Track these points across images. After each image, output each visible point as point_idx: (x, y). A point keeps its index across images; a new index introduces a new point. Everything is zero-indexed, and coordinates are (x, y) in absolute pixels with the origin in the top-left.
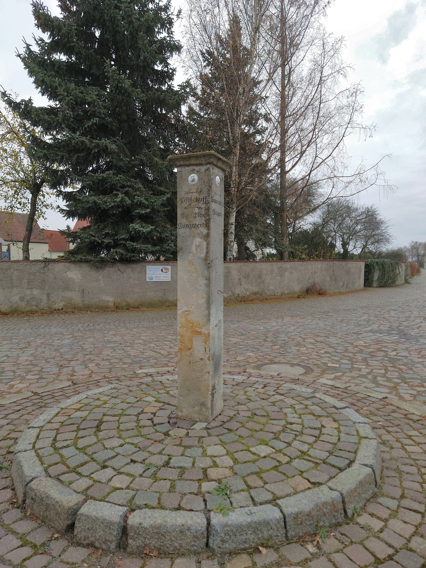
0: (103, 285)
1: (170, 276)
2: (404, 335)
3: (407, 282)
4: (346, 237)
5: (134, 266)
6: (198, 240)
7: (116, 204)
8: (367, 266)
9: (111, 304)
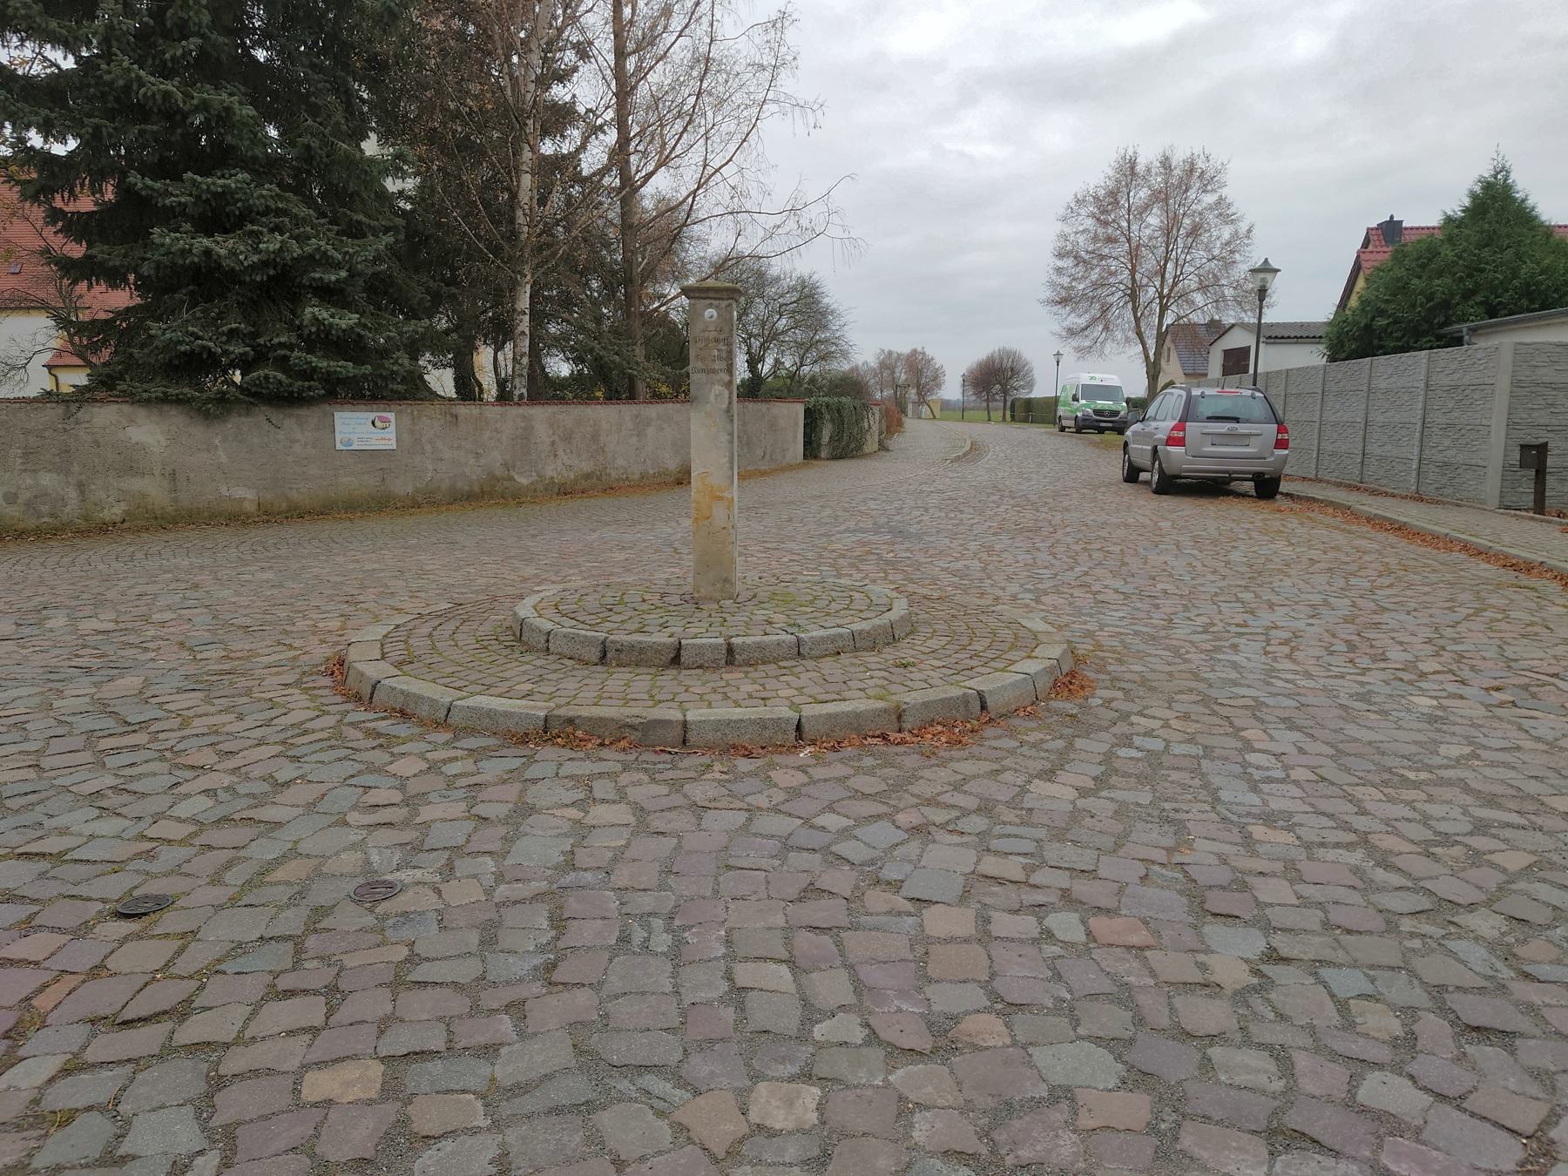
0: (224, 459)
1: (393, 436)
2: (899, 533)
3: (883, 447)
4: (756, 344)
5: (303, 412)
6: (718, 388)
7: (264, 257)
8: (808, 412)
9: (250, 507)
